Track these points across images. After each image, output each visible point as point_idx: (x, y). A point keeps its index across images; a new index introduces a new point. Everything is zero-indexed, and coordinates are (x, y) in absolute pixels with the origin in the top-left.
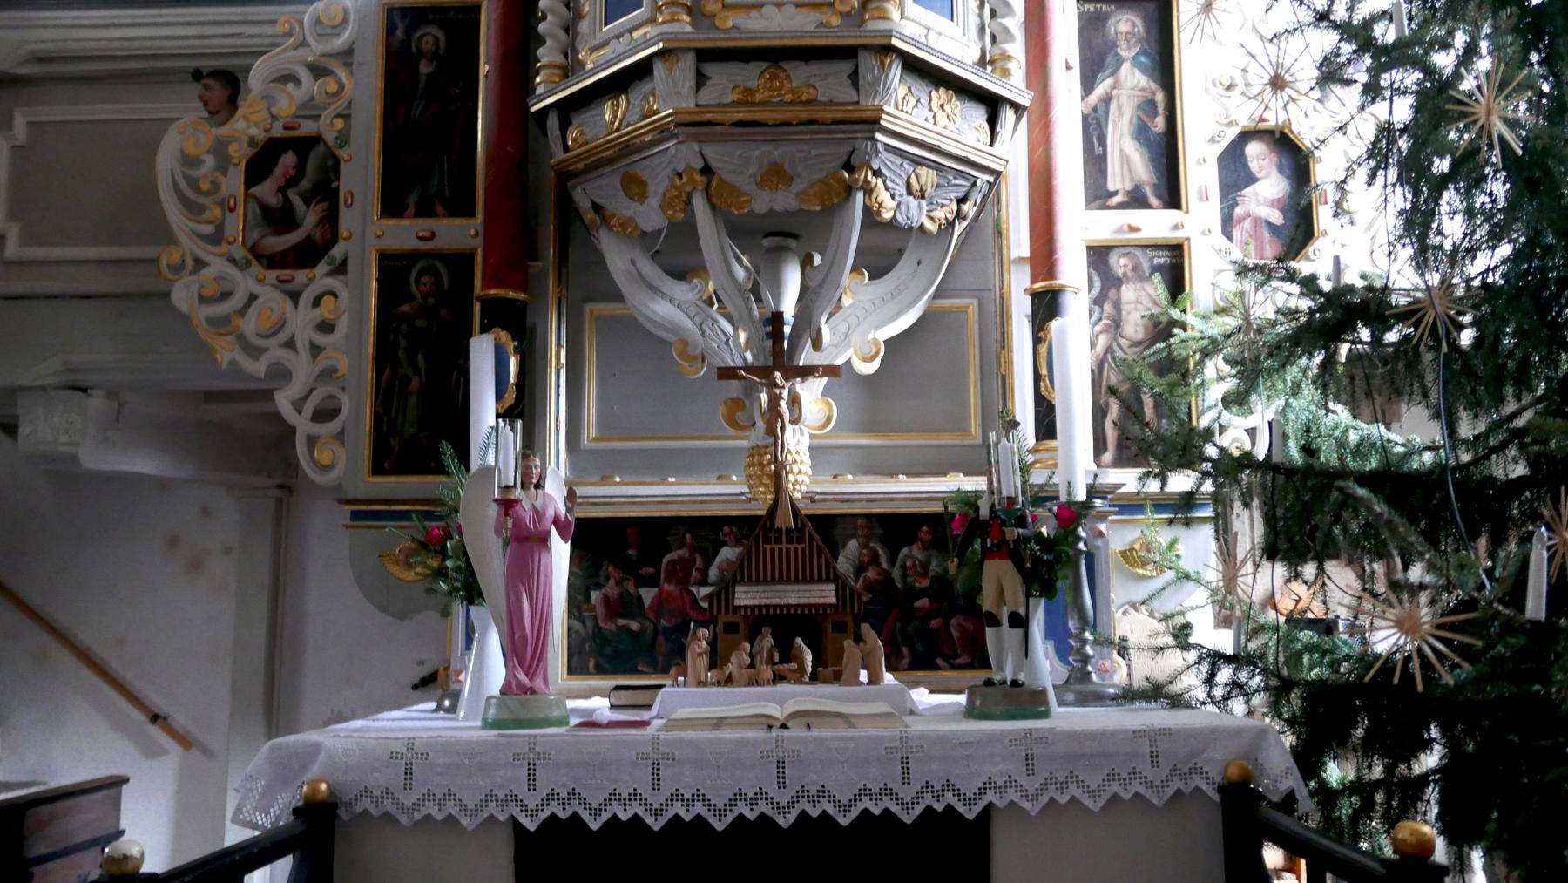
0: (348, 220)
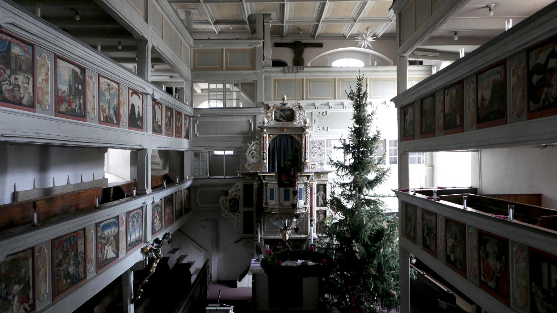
0: (240, 208)
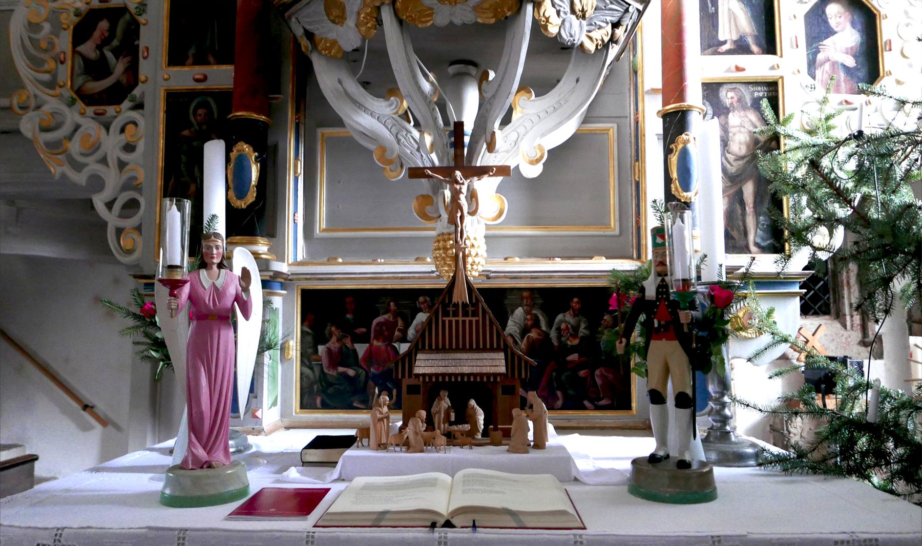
0: (145, 69)
